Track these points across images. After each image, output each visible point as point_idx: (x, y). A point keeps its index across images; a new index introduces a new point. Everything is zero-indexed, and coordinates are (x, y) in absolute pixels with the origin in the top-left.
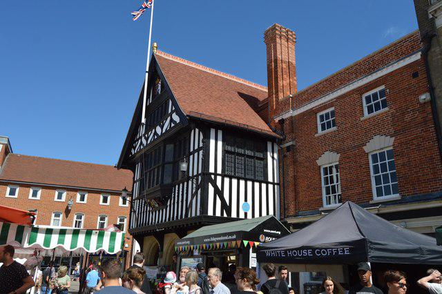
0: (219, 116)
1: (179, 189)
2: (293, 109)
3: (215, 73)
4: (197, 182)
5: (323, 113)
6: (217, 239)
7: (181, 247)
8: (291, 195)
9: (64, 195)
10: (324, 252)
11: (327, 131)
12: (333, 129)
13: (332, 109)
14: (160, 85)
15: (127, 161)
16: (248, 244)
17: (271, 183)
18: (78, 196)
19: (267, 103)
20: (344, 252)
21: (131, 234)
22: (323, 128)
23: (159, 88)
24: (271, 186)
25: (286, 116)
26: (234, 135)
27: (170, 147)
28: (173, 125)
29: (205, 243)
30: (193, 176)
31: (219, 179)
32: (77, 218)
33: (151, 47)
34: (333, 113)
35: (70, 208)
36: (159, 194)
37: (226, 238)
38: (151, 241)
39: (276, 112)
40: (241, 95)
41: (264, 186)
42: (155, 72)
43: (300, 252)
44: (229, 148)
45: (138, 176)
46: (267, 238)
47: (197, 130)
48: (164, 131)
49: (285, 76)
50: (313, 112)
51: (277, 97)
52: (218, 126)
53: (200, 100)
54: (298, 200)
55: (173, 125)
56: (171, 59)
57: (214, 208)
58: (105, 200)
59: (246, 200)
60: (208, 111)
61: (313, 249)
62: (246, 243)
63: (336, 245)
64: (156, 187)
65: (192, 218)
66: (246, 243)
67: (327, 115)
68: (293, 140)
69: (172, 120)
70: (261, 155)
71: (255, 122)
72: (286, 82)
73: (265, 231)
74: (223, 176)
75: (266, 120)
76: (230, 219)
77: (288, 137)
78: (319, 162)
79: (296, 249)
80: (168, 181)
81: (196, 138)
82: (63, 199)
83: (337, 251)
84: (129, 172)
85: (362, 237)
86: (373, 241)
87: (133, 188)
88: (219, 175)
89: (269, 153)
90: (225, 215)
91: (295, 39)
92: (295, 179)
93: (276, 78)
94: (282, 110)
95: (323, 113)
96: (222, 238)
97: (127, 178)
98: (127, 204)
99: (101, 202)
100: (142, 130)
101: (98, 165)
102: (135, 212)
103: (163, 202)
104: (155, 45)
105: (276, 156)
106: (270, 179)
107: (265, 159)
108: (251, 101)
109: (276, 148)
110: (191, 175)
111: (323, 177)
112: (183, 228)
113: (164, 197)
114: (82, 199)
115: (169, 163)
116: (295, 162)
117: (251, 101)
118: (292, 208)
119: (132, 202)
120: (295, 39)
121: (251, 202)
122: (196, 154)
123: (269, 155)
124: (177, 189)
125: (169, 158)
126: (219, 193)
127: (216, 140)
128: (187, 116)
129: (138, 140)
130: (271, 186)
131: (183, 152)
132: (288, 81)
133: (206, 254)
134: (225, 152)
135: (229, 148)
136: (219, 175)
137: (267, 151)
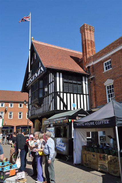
0: (60, 67)
1: (45, 99)
2: (93, 61)
3: (60, 48)
4: (52, 96)
5: (106, 62)
6: (59, 119)
7: (59, 121)
8: (94, 99)
9: (4, 104)
10: (99, 123)
11: (108, 70)
12: (111, 69)
13: (110, 60)
14: (35, 55)
15: (25, 89)
16: (71, 121)
17: (85, 94)
18: (10, 105)
19: (82, 60)
20: (106, 122)
21: (29, 119)
22: (106, 69)
23: (35, 57)
24: (85, 96)
25: (90, 65)
26: (67, 74)
27: (41, 82)
28: (41, 72)
29: (54, 121)
30: (50, 94)
31: (62, 94)
32: (20, 114)
33: (31, 39)
34: (110, 62)
35: (6, 110)
36: (38, 102)
37: (62, 119)
38: (37, 122)
39: (86, 63)
40: (72, 57)
41: (82, 96)
42: (33, 51)
43: (90, 123)
44: (65, 81)
45: (30, 95)
46: (80, 118)
47: (51, 74)
48: (38, 75)
49: (89, 47)
50: (102, 62)
51: (86, 57)
52: (60, 71)
53: (52, 60)
54: (96, 101)
55: (41, 72)
56: (57, 48)
57: (60, 106)
58: (21, 106)
59: (74, 102)
60: (55, 65)
61: (95, 122)
62: (70, 120)
63: (103, 120)
64: (37, 99)
65: (51, 111)
66: (70, 120)
67: (108, 63)
68: (94, 75)
69: (41, 70)
70: (80, 83)
71: (78, 69)
72: (90, 50)
73: (79, 115)
74: (63, 93)
75: (82, 67)
76: (67, 111)
77: (92, 74)
78: (105, 84)
79: (88, 122)
80: (41, 96)
81: (51, 77)
82: (4, 106)
83: (104, 122)
84: (27, 94)
85: (29, 122)
86: (119, 117)
87: (29, 100)
88: (62, 92)
89: (83, 82)
90: (65, 109)
91: (94, 30)
92: (95, 92)
93: (86, 48)
94: (89, 62)
95: (106, 62)
96: (61, 119)
97: (26, 96)
98: (27, 107)
99: (19, 107)
100: (30, 75)
101: (17, 91)
102: (30, 110)
103: (40, 105)
104: (32, 38)
105: (87, 82)
106: (84, 93)
107: (82, 84)
108: (76, 59)
109: (87, 79)
110: (50, 93)
111: (107, 90)
112: (48, 115)
113: (40, 103)
114: (11, 106)
115: (42, 89)
116: (95, 85)
117: (76, 59)
118: (94, 104)
119: (29, 106)
120: (94, 30)
121: (76, 102)
122: (51, 84)
123: (84, 82)
124: (45, 99)
125: (41, 86)
126: (62, 100)
127: (59, 77)
128: (46, 68)
129: (29, 80)
130: (85, 96)
131: (46, 83)
132: (91, 49)
133: (55, 126)
134: (64, 82)
135: (65, 81)
136: (62, 92)
137: (83, 81)
